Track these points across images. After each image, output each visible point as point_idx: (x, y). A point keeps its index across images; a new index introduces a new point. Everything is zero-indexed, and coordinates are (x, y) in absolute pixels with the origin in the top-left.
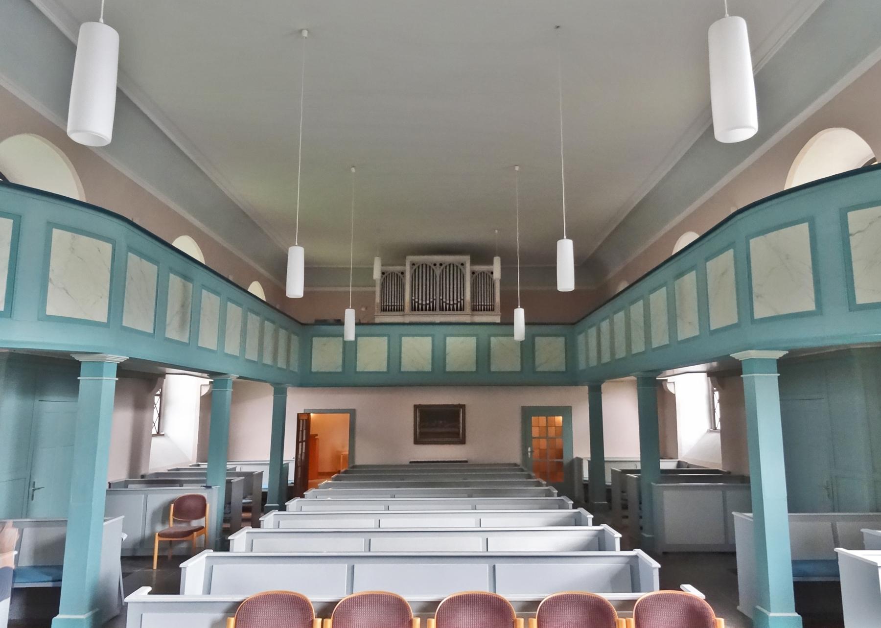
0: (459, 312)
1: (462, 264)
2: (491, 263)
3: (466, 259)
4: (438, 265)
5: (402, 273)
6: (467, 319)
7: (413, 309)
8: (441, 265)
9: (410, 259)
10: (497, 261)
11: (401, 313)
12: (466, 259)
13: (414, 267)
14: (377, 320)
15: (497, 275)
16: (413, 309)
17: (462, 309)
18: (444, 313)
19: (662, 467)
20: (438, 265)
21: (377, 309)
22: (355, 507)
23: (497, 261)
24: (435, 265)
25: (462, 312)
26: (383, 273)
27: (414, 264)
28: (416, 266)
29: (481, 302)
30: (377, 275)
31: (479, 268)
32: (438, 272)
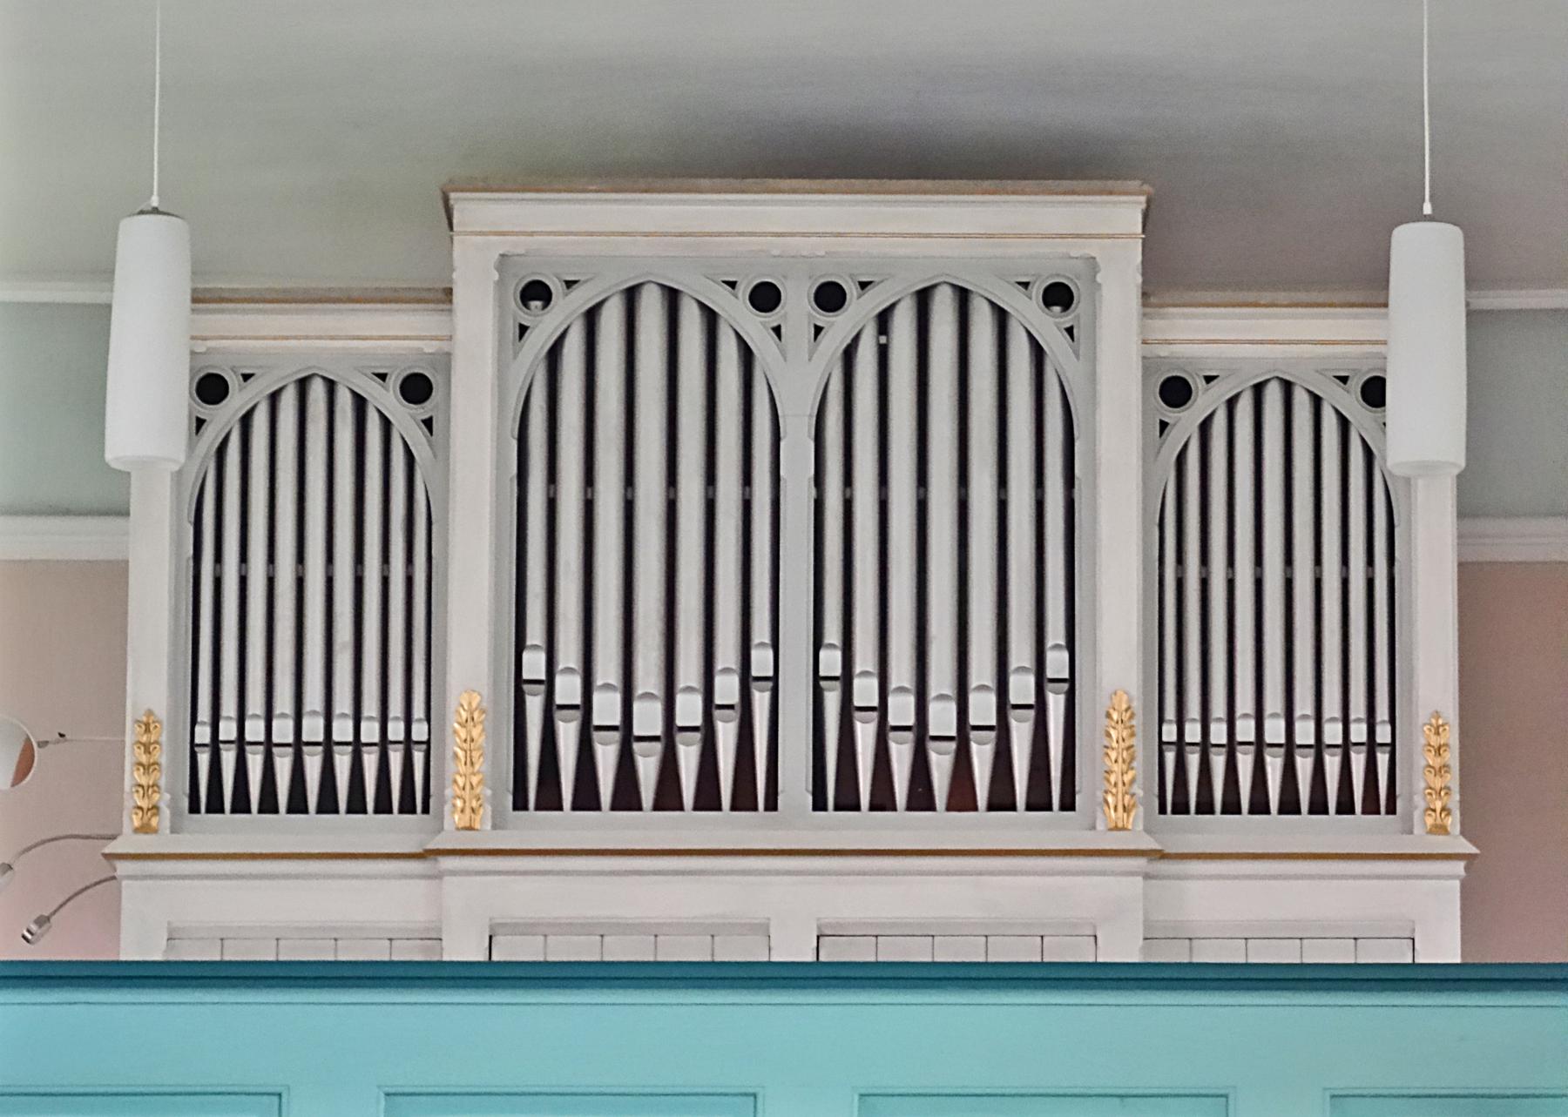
0: (1021, 827)
1: (1058, 296)
2: (1369, 284)
3: (1101, 230)
4: (797, 305)
5: (416, 388)
6: (1109, 913)
7: (533, 786)
8: (830, 297)
9: (503, 228)
10: (1426, 256)
11: (397, 831)
12: (1101, 230)
13: (545, 325)
14: (151, 919)
15: (1424, 432)
16: (533, 786)
17: (1053, 789)
18: (863, 827)
19: (1406, 239)
20: (797, 305)
21: (150, 772)
22: (1198, 294)
23: (1426, 256)
24: (765, 297)
25: (1047, 828)
26: (211, 389)
27: (536, 292)
28: (565, 311)
29: (1248, 716)
30: (145, 420)
31: (1232, 339)
32: (797, 372)
